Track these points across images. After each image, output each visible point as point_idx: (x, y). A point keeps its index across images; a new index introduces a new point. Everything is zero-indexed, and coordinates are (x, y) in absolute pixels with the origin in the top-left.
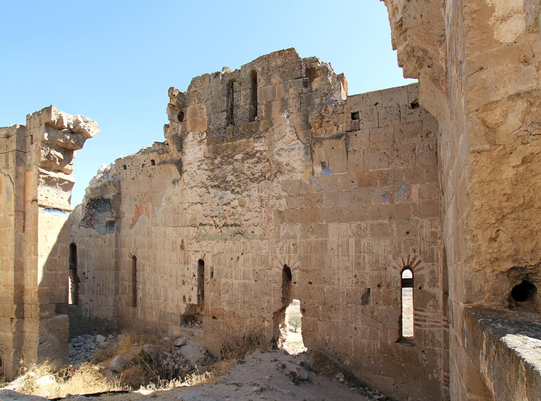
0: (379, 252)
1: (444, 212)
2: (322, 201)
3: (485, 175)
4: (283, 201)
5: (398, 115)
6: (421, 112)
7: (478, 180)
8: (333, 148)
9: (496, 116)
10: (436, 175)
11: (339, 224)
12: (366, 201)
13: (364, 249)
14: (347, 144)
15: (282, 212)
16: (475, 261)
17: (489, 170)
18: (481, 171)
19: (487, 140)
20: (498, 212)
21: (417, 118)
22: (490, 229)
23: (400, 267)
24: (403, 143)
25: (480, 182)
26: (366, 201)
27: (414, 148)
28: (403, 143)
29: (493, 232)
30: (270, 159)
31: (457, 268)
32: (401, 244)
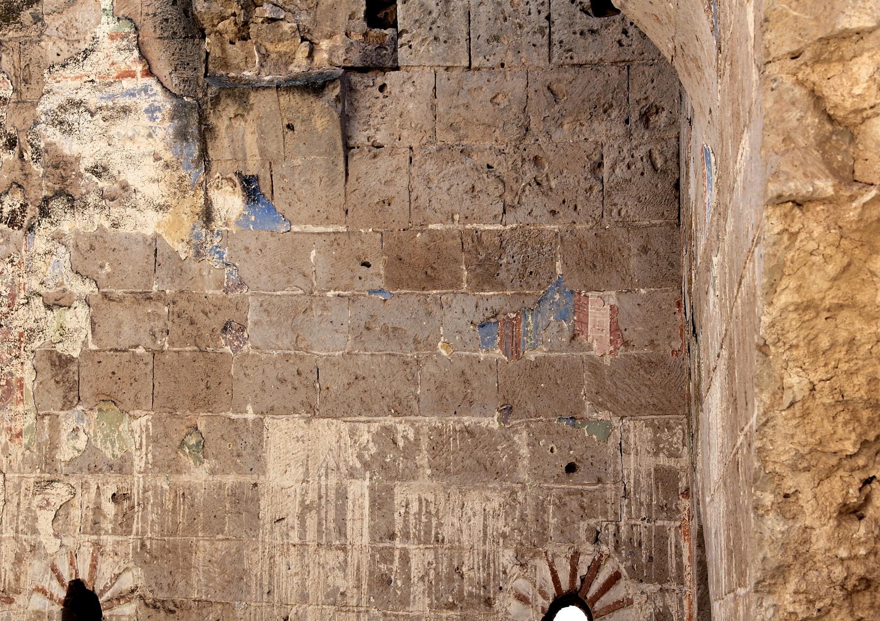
0: (465, 538)
1: (699, 399)
2: (243, 328)
3: (818, 284)
4: (77, 318)
5: (541, 30)
6: (625, 32)
7: (797, 299)
8: (290, 127)
9: (857, 82)
10: (674, 265)
11: (308, 421)
12: (416, 341)
13: (406, 521)
14: (345, 120)
15: (71, 360)
16: (791, 587)
17: (832, 269)
18: (805, 270)
19: (828, 163)
20: (865, 414)
21: (613, 52)
22: (841, 472)
23: (544, 595)
24: (557, 136)
25: (806, 307)
26: (416, 341)
27: (596, 158)
28: (557, 136)
29: (849, 485)
30: (22, 139)
31: (736, 611)
32: (545, 511)
